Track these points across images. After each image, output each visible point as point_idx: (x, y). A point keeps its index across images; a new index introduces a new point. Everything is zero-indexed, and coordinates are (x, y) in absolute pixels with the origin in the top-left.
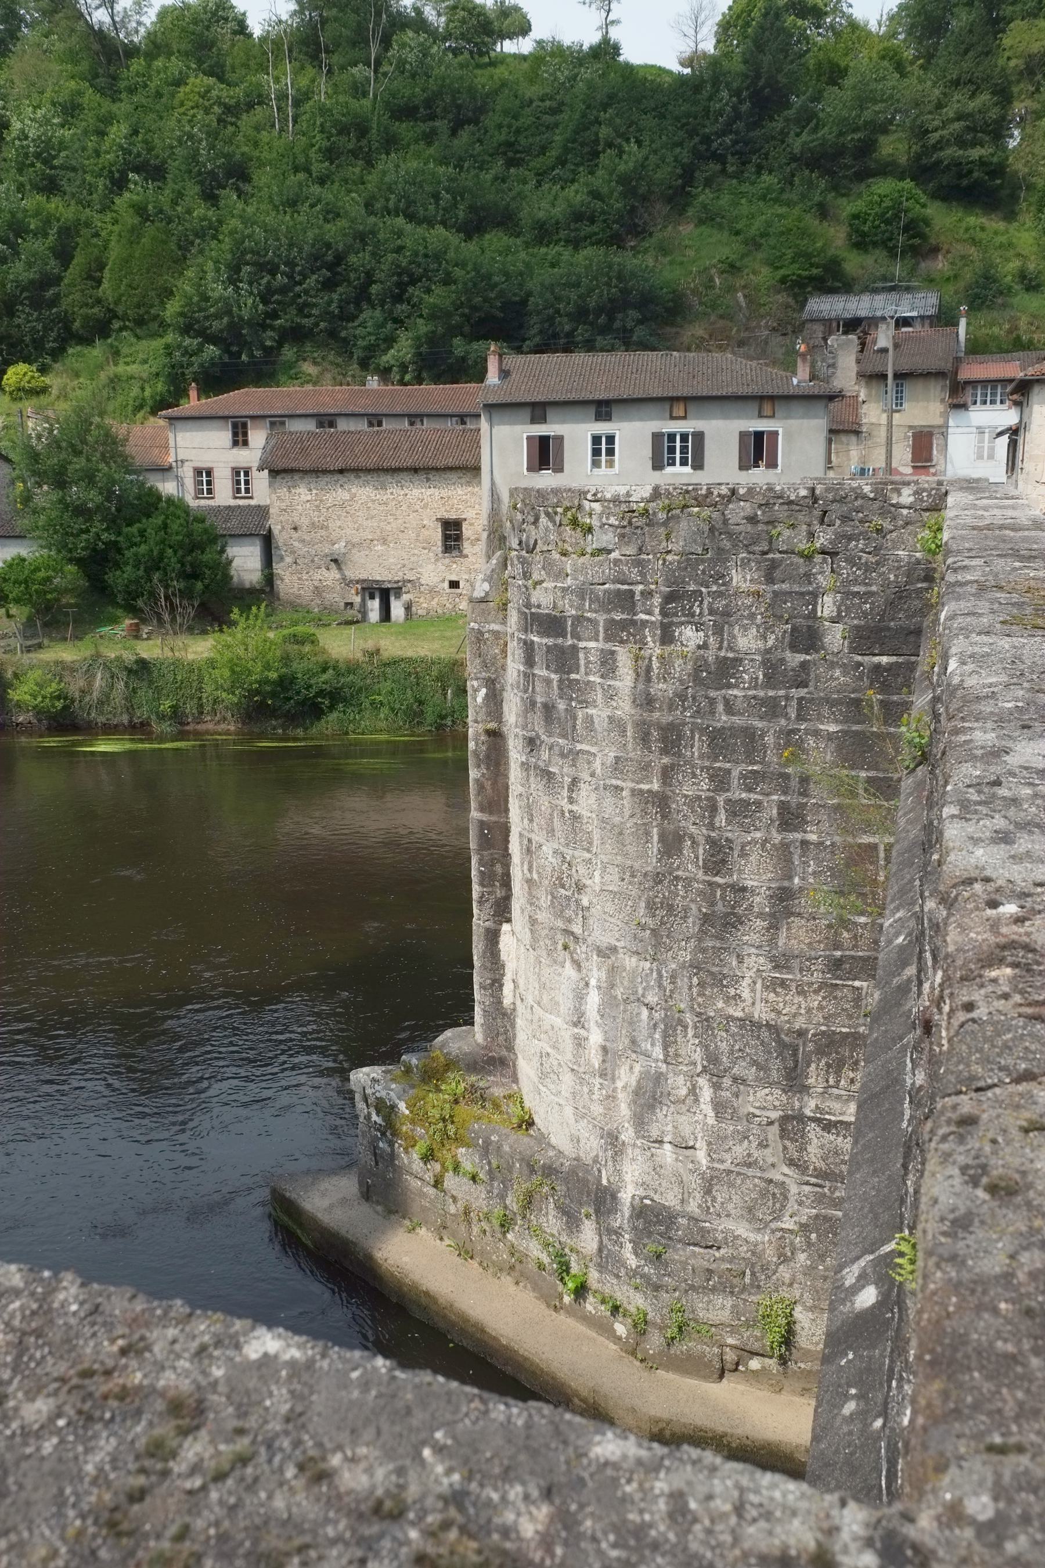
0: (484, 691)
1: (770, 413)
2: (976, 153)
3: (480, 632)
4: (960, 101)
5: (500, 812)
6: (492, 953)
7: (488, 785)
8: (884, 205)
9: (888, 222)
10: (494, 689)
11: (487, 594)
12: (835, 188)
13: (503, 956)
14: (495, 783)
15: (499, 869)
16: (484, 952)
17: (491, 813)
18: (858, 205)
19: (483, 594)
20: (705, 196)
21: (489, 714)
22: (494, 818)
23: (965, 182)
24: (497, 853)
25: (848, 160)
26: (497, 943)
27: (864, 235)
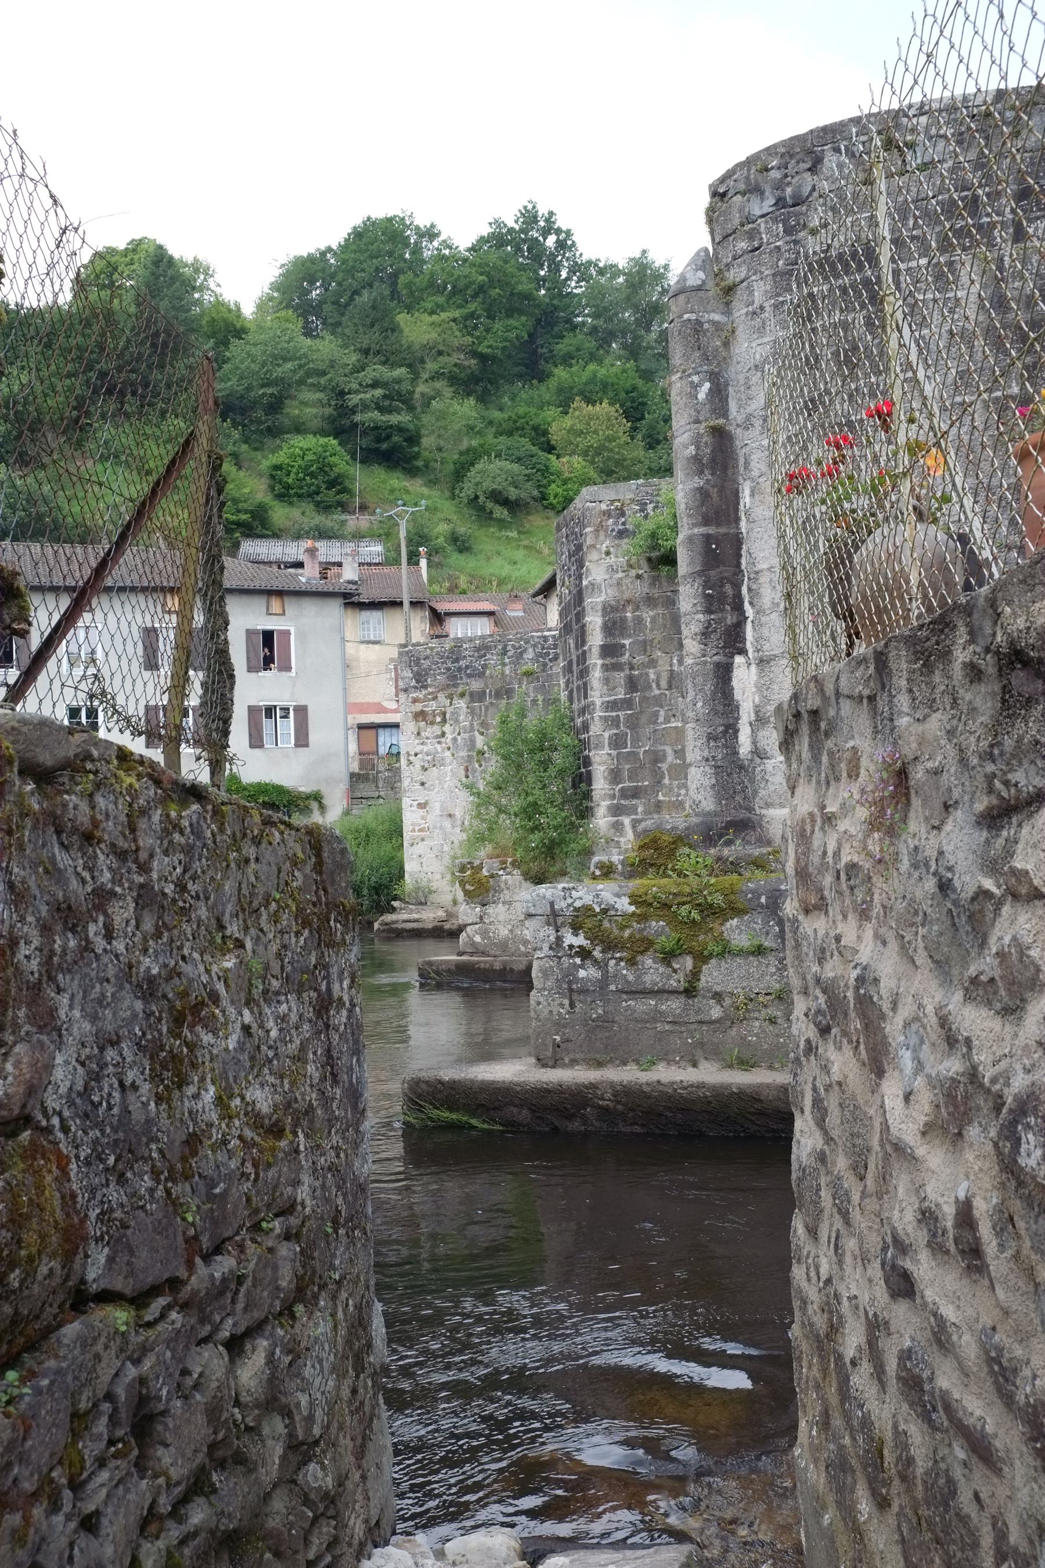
0: (707, 385)
1: (279, 611)
2: (394, 419)
3: (699, 322)
4: (377, 371)
5: (729, 523)
6: (724, 693)
7: (714, 492)
8: (306, 458)
9: (312, 475)
10: (718, 384)
11: (704, 282)
12: (246, 441)
13: (738, 695)
14: (722, 490)
15: (728, 589)
16: (714, 693)
17: (718, 525)
18: (280, 457)
19: (700, 282)
20: (106, 431)
21: (713, 411)
22: (722, 530)
23: (384, 446)
24: (727, 571)
25: (259, 413)
26: (730, 679)
27: (288, 487)
